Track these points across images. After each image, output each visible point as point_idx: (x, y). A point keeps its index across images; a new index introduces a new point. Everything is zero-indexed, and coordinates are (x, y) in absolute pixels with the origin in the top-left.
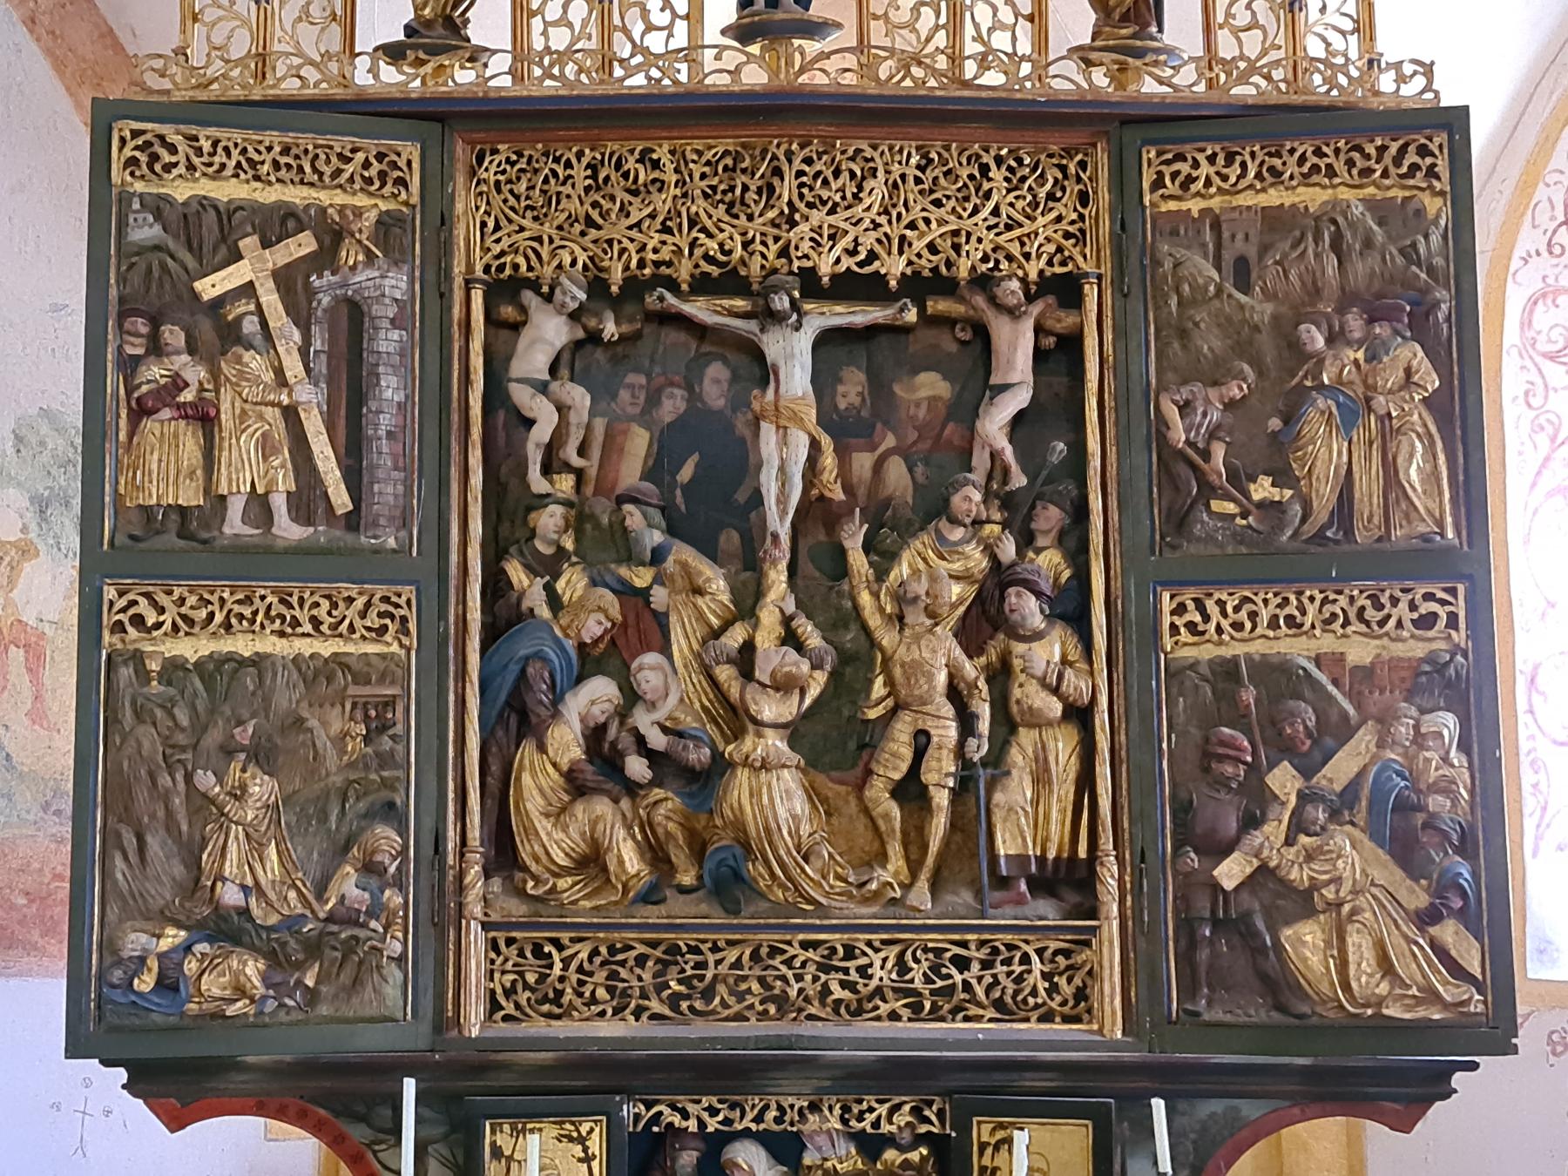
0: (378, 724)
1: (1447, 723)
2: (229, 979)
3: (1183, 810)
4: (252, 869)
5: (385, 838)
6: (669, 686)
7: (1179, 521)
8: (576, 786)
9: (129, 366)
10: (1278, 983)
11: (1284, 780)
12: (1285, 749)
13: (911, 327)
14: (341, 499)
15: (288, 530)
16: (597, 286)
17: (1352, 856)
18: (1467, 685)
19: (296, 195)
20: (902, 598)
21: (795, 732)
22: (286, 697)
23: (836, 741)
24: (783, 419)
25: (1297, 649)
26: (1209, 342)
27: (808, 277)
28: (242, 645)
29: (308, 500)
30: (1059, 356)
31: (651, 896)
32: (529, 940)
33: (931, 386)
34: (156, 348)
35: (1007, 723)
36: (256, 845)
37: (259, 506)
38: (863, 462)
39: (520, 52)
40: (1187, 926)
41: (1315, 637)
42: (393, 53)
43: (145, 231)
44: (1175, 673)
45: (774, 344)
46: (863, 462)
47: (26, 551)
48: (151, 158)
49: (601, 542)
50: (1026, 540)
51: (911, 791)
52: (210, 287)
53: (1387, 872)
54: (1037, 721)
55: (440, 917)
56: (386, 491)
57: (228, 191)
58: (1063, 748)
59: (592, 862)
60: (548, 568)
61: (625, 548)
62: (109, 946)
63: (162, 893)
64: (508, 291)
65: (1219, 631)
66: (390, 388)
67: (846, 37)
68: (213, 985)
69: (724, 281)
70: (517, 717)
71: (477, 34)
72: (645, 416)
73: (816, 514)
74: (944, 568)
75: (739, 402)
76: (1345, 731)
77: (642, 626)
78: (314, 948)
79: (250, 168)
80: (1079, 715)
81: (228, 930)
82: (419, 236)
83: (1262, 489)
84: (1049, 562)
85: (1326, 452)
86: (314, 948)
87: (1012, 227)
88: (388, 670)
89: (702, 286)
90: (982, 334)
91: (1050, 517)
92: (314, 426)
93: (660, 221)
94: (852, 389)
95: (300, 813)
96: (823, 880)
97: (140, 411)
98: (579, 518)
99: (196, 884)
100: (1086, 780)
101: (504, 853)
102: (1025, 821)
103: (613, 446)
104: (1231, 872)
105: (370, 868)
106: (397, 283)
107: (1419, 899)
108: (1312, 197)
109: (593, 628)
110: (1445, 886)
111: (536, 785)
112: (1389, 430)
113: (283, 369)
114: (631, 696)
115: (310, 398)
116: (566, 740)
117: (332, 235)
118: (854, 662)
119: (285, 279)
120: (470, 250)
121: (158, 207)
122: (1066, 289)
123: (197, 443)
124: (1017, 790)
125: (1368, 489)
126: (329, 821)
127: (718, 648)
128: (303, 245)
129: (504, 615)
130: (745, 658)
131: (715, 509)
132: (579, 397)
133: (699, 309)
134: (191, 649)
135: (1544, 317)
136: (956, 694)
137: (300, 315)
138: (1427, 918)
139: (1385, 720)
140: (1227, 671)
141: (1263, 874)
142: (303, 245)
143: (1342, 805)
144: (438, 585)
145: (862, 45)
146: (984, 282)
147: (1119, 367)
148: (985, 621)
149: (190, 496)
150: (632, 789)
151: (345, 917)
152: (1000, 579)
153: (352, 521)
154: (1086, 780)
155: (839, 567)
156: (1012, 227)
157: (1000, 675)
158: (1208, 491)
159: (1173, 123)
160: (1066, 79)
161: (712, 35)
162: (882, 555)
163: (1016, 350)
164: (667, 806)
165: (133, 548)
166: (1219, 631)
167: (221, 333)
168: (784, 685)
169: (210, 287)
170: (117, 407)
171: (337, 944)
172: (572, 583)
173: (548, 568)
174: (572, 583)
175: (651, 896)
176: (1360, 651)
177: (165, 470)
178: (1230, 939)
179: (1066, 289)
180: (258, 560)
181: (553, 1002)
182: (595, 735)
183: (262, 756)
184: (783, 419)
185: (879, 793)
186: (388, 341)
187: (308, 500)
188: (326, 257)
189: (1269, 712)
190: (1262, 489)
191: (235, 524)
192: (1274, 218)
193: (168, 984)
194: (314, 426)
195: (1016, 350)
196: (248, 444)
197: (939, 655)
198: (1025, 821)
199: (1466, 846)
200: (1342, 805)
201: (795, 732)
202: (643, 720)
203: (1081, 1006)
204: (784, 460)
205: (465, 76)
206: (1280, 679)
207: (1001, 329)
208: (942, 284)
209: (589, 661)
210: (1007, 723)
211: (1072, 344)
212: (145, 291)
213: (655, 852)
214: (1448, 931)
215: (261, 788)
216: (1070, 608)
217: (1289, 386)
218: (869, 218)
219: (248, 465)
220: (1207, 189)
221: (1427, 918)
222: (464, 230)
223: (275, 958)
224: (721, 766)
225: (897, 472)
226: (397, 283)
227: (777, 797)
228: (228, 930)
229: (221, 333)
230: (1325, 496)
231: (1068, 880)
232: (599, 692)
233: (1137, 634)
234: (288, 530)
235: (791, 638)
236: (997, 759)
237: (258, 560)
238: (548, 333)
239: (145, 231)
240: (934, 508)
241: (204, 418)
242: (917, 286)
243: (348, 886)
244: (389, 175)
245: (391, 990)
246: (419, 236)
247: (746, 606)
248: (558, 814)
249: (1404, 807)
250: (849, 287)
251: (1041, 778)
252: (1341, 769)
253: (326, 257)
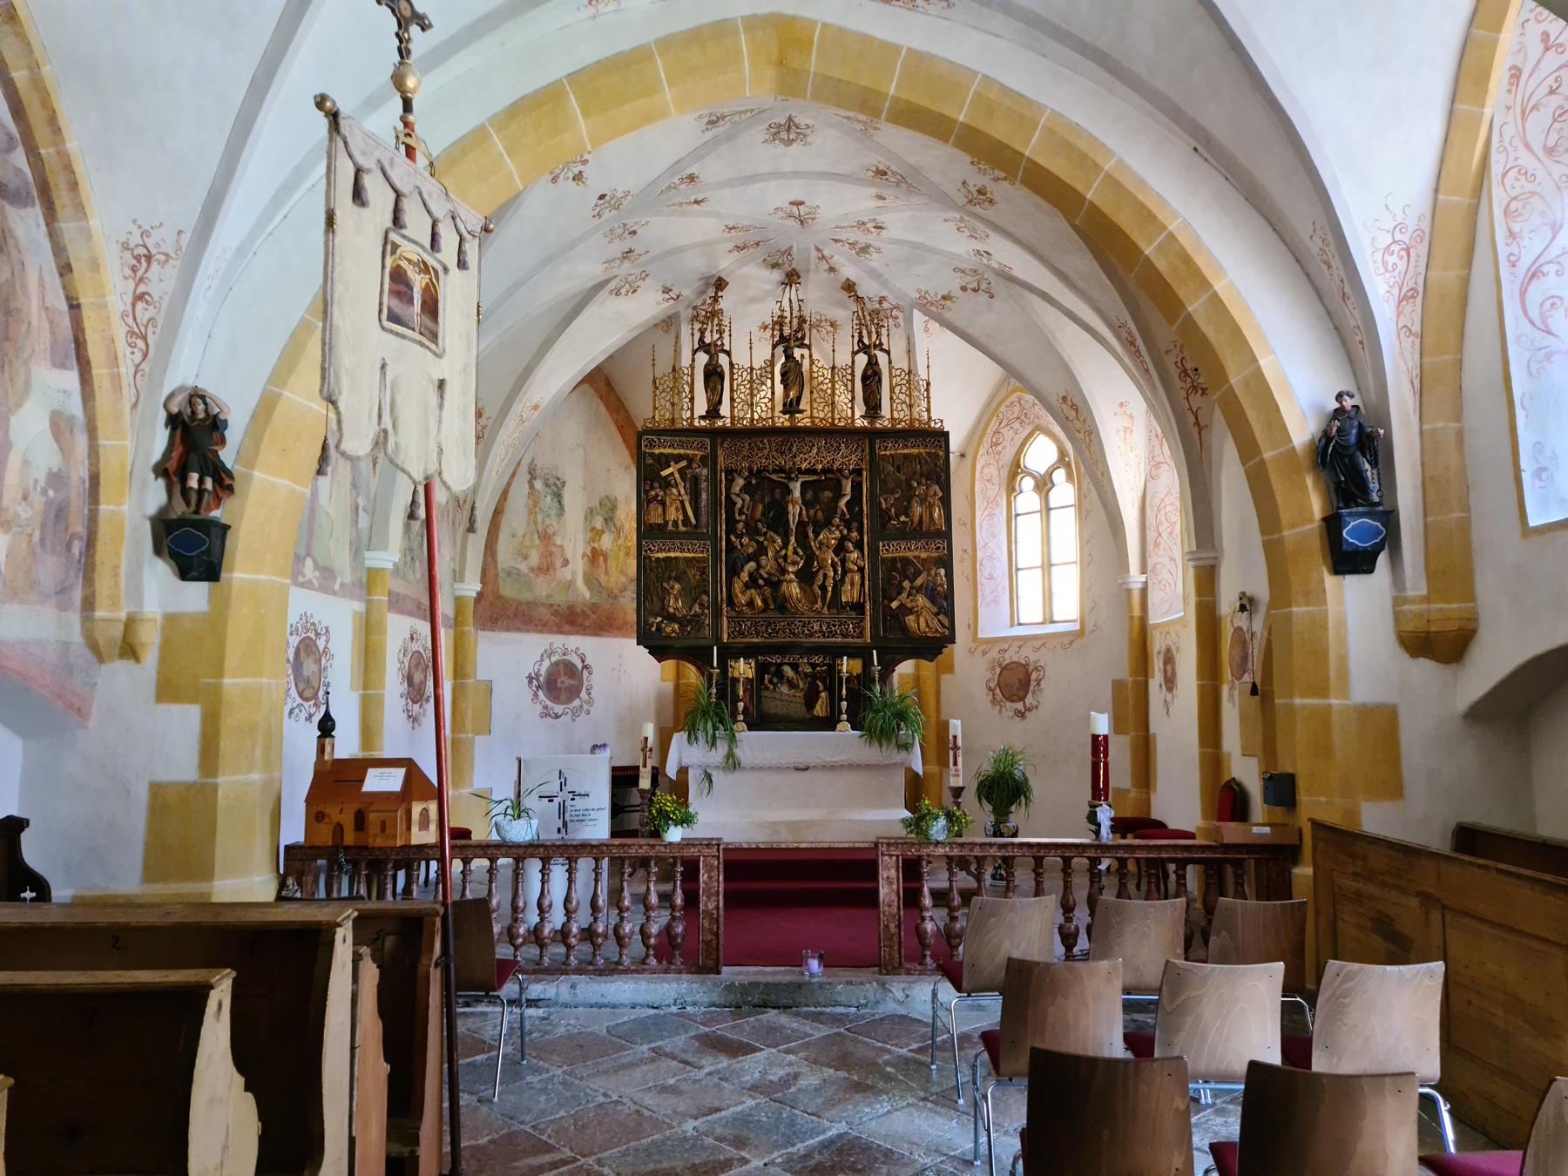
0: (703, 572)
1: (942, 571)
2: (672, 628)
3: (884, 590)
4: (675, 604)
5: (705, 598)
6: (768, 563)
7: (884, 526)
8: (747, 586)
9: (647, 492)
10: (904, 628)
11: (906, 584)
12: (906, 577)
13: (823, 484)
14: (693, 521)
15: (682, 528)
16: (750, 471)
17: (921, 600)
18: (946, 562)
19: (682, 451)
20: (821, 543)
21: (796, 574)
22: (682, 566)
23: (806, 577)
24: (794, 503)
25: (909, 554)
26: (891, 485)
27: (799, 470)
28: (672, 554)
29: (686, 521)
30: (857, 487)
31: (764, 611)
32: (736, 620)
33: (828, 494)
34: (652, 488)
35: (845, 572)
36: (676, 600)
37: (675, 523)
38: (812, 512)
39: (733, 417)
40: (885, 617)
41: (916, 551)
42: (702, 417)
43: (650, 461)
44: (883, 560)
45: (791, 485)
46: (812, 512)
47: (603, 532)
48: (651, 445)
49: (752, 531)
50: (849, 530)
51: (823, 587)
52: (664, 473)
53: (928, 604)
54: (851, 571)
55: (717, 615)
56: (704, 519)
57: (668, 451)
58: (857, 578)
59: (751, 603)
60: (740, 537)
61: (758, 532)
62: (646, 621)
63: (657, 609)
64: (731, 473)
65: (891, 550)
66: (704, 496)
67: (808, 413)
68: (668, 630)
69: (781, 470)
70: (733, 571)
71: (722, 413)
72: (762, 501)
73: (801, 525)
74: (831, 536)
75: (783, 497)
76: (920, 573)
77: (762, 550)
78: (689, 622)
79: (672, 446)
80: (861, 570)
81: (671, 618)
82: (710, 460)
83: (903, 518)
84: (855, 534)
85: (917, 510)
86: (689, 622)
87: (846, 457)
88: (705, 560)
89: (775, 471)
90: (839, 482)
91: (855, 524)
92: (687, 504)
93: (767, 457)
94: (809, 495)
95: (684, 593)
96: (803, 607)
97: (649, 502)
98: (747, 525)
99: (664, 607)
100: (862, 584)
101: (731, 601)
102: (849, 594)
103: (754, 508)
104: (894, 605)
105: (701, 605)
106: (705, 472)
107: (935, 610)
108: (915, 451)
109: (751, 550)
110: (941, 607)
111: (738, 586)
112: (931, 506)
113: (680, 491)
114: (759, 566)
115: (686, 498)
116: (745, 576)
117: (690, 460)
118: (810, 557)
119: (680, 471)
120: (721, 462)
121: (652, 455)
122: (858, 472)
123: (16, 240)
124: (848, 586)
125: (926, 518)
126: (693, 593)
127: (781, 554)
128: (684, 463)
129: (730, 547)
130: (785, 557)
131: (778, 522)
132: (747, 497)
133: (774, 477)
134: (661, 555)
135: (986, 471)
136: (833, 565)
137: (684, 479)
138: (936, 614)
139: (929, 571)
140: (894, 559)
141: (902, 605)
142: (684, 463)
143: (919, 590)
144: (715, 540)
145: (812, 417)
146: (840, 470)
147: (871, 490)
148: (840, 549)
149: (660, 521)
150: (759, 587)
151: (696, 615)
152: (843, 539)
153: (696, 526)
154: (862, 584)
155: (807, 537)
156: (846, 457)
157: (843, 561)
158: (891, 519)
159: (885, 434)
160: (859, 423)
161: (777, 413)
162: (817, 534)
163: (848, 487)
164: (768, 590)
165: (648, 532)
166: (891, 550)
167: (667, 484)
168: (794, 563)
169: (664, 473)
170: (643, 502)
171: (696, 621)
172: (745, 540)
173: (740, 537)
174: (745, 540)
175: (764, 611)
176: (924, 555)
177: (655, 517)
178: (892, 621)
179: (858, 472)
180: (675, 535)
181: (742, 634)
182: (751, 575)
183: (677, 579)
184: (794, 503)
185: (815, 587)
186: (704, 485)
187: (686, 521)
188: (689, 466)
189: (906, 568)
190: (903, 518)
191: (670, 527)
192: (905, 455)
193: (659, 629)
194: (687, 504)
195: (848, 487)
196: (673, 509)
197: (830, 557)
198: (849, 594)
199: (946, 598)
200: (919, 590)
201: (796, 574)
202: (762, 572)
203: (861, 635)
204: (794, 511)
205: (720, 423)
206: (905, 560)
207: (844, 481)
208: (830, 471)
209: (750, 558)
210: (845, 572)
211: (860, 484)
212: (649, 477)
213: (764, 601)
214: (941, 617)
215: (677, 586)
216: (859, 545)
217: (909, 496)
218: (812, 457)
219: (673, 514)
220: (889, 450)
221: (936, 614)
222: (721, 459)
223: (681, 625)
224: (780, 582)
225: (820, 514)
226: (705, 472)
227: (794, 589)
228: (671, 618)
229: (667, 484)
230: (916, 519)
231: (858, 607)
232: (752, 564)
233: (874, 551)
234: (682, 528)
235: (795, 552)
236: (842, 581)
237: (675, 535)
238: (740, 482)
239: (650, 461)
240: (828, 523)
241: (663, 503)
242: (824, 471)
243: (697, 608)
244: (703, 446)
245: (707, 632)
246: (710, 460)
247: (785, 545)
248: (743, 593)
249: (933, 590)
250: (808, 472)
251: (852, 584)
252: (919, 581)
253: (689, 466)
